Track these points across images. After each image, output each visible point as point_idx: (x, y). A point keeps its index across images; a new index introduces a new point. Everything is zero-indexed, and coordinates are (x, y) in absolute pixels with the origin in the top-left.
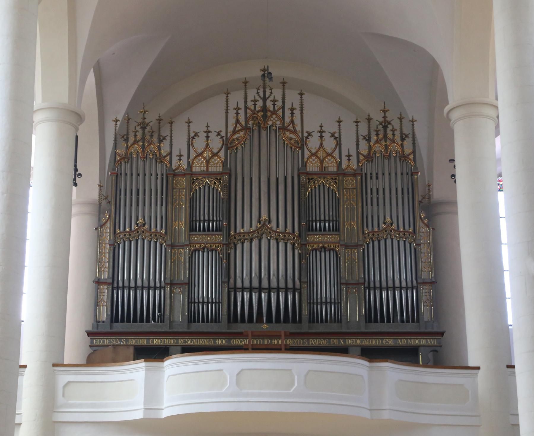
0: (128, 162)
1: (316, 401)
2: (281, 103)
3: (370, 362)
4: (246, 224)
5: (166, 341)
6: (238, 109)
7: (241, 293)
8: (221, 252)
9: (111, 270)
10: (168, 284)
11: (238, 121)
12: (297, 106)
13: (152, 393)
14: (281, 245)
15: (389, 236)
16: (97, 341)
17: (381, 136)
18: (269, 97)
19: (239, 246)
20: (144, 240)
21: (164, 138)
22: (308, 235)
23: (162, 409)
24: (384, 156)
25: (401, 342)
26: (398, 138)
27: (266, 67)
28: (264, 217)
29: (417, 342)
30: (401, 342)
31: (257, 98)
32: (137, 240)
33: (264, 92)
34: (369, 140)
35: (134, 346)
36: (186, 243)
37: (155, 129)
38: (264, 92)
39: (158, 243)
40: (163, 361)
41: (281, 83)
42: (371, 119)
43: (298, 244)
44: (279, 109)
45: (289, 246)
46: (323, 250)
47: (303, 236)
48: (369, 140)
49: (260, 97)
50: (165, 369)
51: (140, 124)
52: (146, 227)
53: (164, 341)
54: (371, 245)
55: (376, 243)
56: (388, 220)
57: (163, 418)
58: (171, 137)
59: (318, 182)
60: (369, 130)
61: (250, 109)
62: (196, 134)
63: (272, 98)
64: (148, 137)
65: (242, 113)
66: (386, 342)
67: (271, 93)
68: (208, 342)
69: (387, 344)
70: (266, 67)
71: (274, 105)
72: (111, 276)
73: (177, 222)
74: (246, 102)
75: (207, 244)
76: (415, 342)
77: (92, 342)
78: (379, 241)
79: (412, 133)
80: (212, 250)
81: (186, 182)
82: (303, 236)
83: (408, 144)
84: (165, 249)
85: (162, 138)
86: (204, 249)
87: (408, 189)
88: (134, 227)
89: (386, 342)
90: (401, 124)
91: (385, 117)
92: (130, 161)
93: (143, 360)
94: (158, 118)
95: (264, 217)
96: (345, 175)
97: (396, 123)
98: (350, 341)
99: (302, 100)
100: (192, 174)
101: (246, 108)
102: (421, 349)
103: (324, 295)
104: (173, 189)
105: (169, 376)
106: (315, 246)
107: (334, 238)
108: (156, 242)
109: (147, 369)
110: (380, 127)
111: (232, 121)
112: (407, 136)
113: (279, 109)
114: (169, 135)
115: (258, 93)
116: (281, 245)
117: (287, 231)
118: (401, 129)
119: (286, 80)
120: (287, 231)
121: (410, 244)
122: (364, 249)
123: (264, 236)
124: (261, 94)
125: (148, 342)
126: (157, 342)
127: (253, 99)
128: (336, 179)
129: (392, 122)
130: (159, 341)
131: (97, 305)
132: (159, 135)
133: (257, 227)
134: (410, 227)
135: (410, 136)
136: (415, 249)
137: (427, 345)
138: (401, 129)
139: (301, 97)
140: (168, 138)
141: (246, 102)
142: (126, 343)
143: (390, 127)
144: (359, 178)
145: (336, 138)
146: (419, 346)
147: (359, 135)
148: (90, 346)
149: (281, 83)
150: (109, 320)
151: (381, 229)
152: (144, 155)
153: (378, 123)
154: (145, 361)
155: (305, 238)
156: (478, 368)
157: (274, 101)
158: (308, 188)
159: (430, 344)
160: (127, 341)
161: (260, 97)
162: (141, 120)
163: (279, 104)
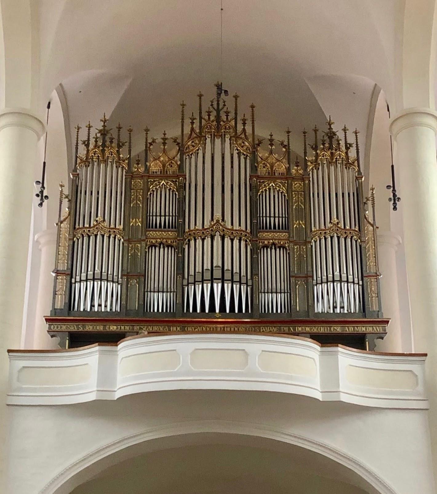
0: (89, 166)
1: (146, 381)
2: (234, 115)
3: (322, 347)
4: (197, 221)
5: (123, 327)
6: (193, 119)
7: (220, 285)
8: (177, 248)
9: (70, 262)
10: (124, 275)
11: (192, 129)
12: (248, 117)
13: (106, 375)
14: (236, 242)
15: (335, 235)
16: (55, 327)
17: (327, 145)
18: (223, 108)
19: (192, 242)
20: (103, 236)
21: (123, 145)
22: (259, 232)
23: (115, 391)
24: (330, 163)
25: (349, 329)
26: (344, 149)
27: (220, 84)
28: (218, 215)
29: (364, 329)
30: (349, 329)
31: (211, 109)
32: (96, 236)
33: (218, 104)
34: (87, 146)
35: (69, 332)
36: (142, 239)
37: (115, 136)
38: (218, 104)
39: (116, 239)
40: (117, 346)
41: (198, 95)
42: (317, 130)
43: (250, 241)
44: (231, 120)
45: (243, 243)
46: (162, 246)
47: (255, 232)
48: (87, 146)
49: (214, 108)
50: (119, 353)
51: (100, 131)
52: (106, 224)
53: (121, 328)
54: (80, 241)
55: (323, 241)
56: (335, 220)
57: (116, 399)
58: (130, 143)
59: (269, 185)
60: (89, 136)
61: (204, 119)
62: (154, 141)
63: (225, 109)
64: (108, 143)
65: (197, 122)
66: (334, 329)
67: (224, 105)
68: (163, 329)
69: (334, 332)
70: (220, 84)
71: (227, 116)
72: (70, 267)
73: (134, 220)
74: (200, 113)
75: (163, 239)
76: (361, 329)
77: (50, 328)
78: (89, 237)
79: (355, 143)
80: (172, 247)
81: (143, 183)
82: (255, 232)
83: (352, 154)
84: (123, 243)
85: (121, 144)
86: (160, 244)
87: (353, 193)
88: (329, 225)
89: (334, 329)
90: (345, 135)
91: (104, 126)
92: (91, 165)
93: (97, 344)
94: (118, 126)
95: (218, 215)
96: (293, 179)
97: (340, 135)
98: (300, 329)
99: (253, 112)
100: (149, 176)
101: (201, 118)
102: (368, 336)
103: (156, 285)
104: (131, 189)
105: (122, 359)
106: (266, 242)
107: (284, 235)
108: (115, 238)
109: (101, 352)
110: (326, 138)
111: (187, 130)
112: (351, 145)
113: (231, 120)
114: (128, 141)
115: (212, 105)
116: (236, 242)
117: (111, 227)
118: (346, 139)
119: (238, 94)
120: (111, 227)
121: (356, 241)
122: (312, 246)
123: (218, 233)
124: (215, 106)
125: (104, 328)
126: (113, 328)
127: (207, 110)
128: (176, 181)
129: (337, 133)
130: (115, 327)
131: (56, 294)
132: (119, 141)
133: (211, 224)
134: (120, 224)
135: (354, 145)
136: (360, 246)
137: (373, 332)
138: (346, 139)
139: (253, 110)
140: (127, 144)
141: (200, 113)
142: (83, 329)
143: (335, 137)
144: (307, 182)
145: (178, 144)
146: (366, 334)
147: (307, 144)
148: (48, 331)
149: (198, 95)
150: (67, 308)
151: (92, 225)
152: (103, 158)
153: (97, 131)
154: (99, 345)
155: (257, 235)
156: (426, 355)
157: (227, 113)
158: (259, 190)
159: (376, 332)
160: (84, 326)
161: (214, 108)
162: (102, 128)
163: (232, 116)
